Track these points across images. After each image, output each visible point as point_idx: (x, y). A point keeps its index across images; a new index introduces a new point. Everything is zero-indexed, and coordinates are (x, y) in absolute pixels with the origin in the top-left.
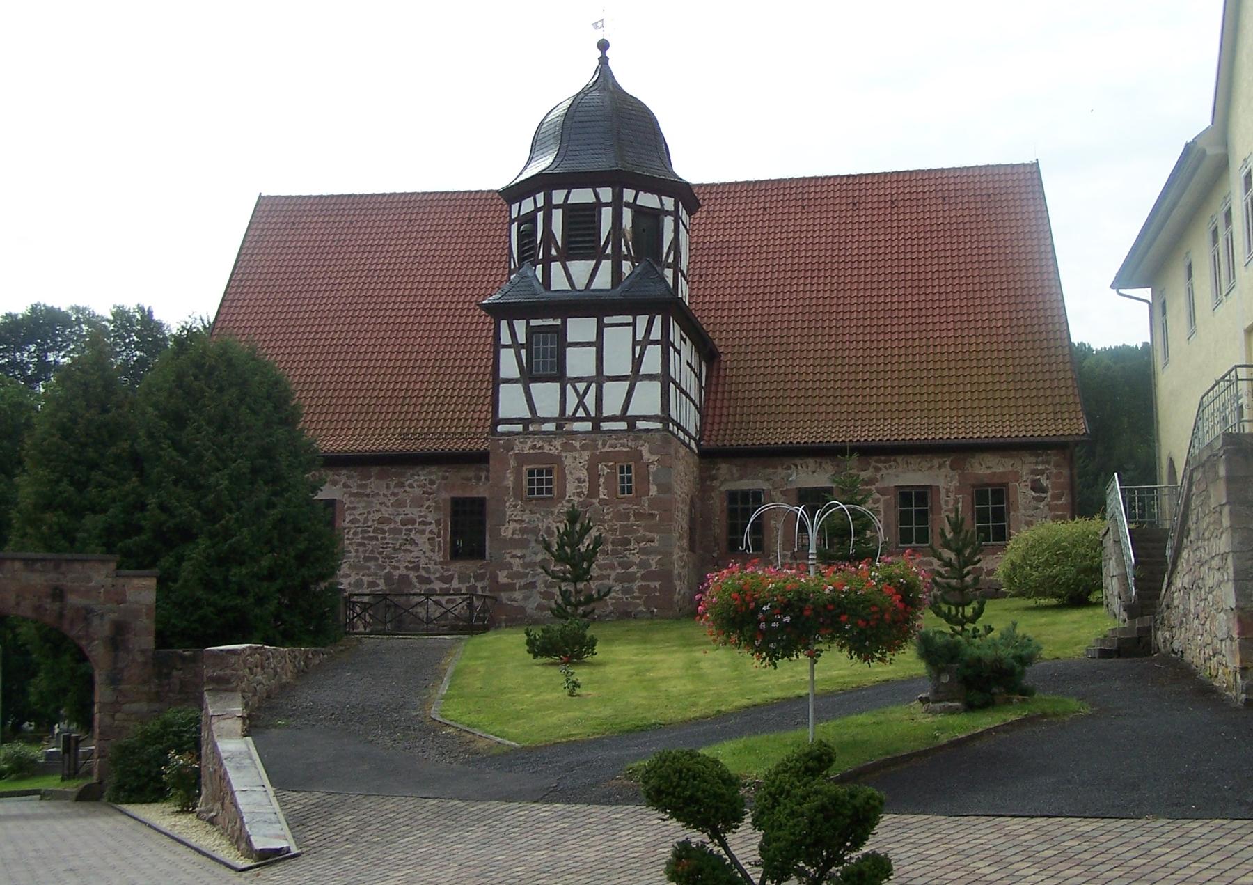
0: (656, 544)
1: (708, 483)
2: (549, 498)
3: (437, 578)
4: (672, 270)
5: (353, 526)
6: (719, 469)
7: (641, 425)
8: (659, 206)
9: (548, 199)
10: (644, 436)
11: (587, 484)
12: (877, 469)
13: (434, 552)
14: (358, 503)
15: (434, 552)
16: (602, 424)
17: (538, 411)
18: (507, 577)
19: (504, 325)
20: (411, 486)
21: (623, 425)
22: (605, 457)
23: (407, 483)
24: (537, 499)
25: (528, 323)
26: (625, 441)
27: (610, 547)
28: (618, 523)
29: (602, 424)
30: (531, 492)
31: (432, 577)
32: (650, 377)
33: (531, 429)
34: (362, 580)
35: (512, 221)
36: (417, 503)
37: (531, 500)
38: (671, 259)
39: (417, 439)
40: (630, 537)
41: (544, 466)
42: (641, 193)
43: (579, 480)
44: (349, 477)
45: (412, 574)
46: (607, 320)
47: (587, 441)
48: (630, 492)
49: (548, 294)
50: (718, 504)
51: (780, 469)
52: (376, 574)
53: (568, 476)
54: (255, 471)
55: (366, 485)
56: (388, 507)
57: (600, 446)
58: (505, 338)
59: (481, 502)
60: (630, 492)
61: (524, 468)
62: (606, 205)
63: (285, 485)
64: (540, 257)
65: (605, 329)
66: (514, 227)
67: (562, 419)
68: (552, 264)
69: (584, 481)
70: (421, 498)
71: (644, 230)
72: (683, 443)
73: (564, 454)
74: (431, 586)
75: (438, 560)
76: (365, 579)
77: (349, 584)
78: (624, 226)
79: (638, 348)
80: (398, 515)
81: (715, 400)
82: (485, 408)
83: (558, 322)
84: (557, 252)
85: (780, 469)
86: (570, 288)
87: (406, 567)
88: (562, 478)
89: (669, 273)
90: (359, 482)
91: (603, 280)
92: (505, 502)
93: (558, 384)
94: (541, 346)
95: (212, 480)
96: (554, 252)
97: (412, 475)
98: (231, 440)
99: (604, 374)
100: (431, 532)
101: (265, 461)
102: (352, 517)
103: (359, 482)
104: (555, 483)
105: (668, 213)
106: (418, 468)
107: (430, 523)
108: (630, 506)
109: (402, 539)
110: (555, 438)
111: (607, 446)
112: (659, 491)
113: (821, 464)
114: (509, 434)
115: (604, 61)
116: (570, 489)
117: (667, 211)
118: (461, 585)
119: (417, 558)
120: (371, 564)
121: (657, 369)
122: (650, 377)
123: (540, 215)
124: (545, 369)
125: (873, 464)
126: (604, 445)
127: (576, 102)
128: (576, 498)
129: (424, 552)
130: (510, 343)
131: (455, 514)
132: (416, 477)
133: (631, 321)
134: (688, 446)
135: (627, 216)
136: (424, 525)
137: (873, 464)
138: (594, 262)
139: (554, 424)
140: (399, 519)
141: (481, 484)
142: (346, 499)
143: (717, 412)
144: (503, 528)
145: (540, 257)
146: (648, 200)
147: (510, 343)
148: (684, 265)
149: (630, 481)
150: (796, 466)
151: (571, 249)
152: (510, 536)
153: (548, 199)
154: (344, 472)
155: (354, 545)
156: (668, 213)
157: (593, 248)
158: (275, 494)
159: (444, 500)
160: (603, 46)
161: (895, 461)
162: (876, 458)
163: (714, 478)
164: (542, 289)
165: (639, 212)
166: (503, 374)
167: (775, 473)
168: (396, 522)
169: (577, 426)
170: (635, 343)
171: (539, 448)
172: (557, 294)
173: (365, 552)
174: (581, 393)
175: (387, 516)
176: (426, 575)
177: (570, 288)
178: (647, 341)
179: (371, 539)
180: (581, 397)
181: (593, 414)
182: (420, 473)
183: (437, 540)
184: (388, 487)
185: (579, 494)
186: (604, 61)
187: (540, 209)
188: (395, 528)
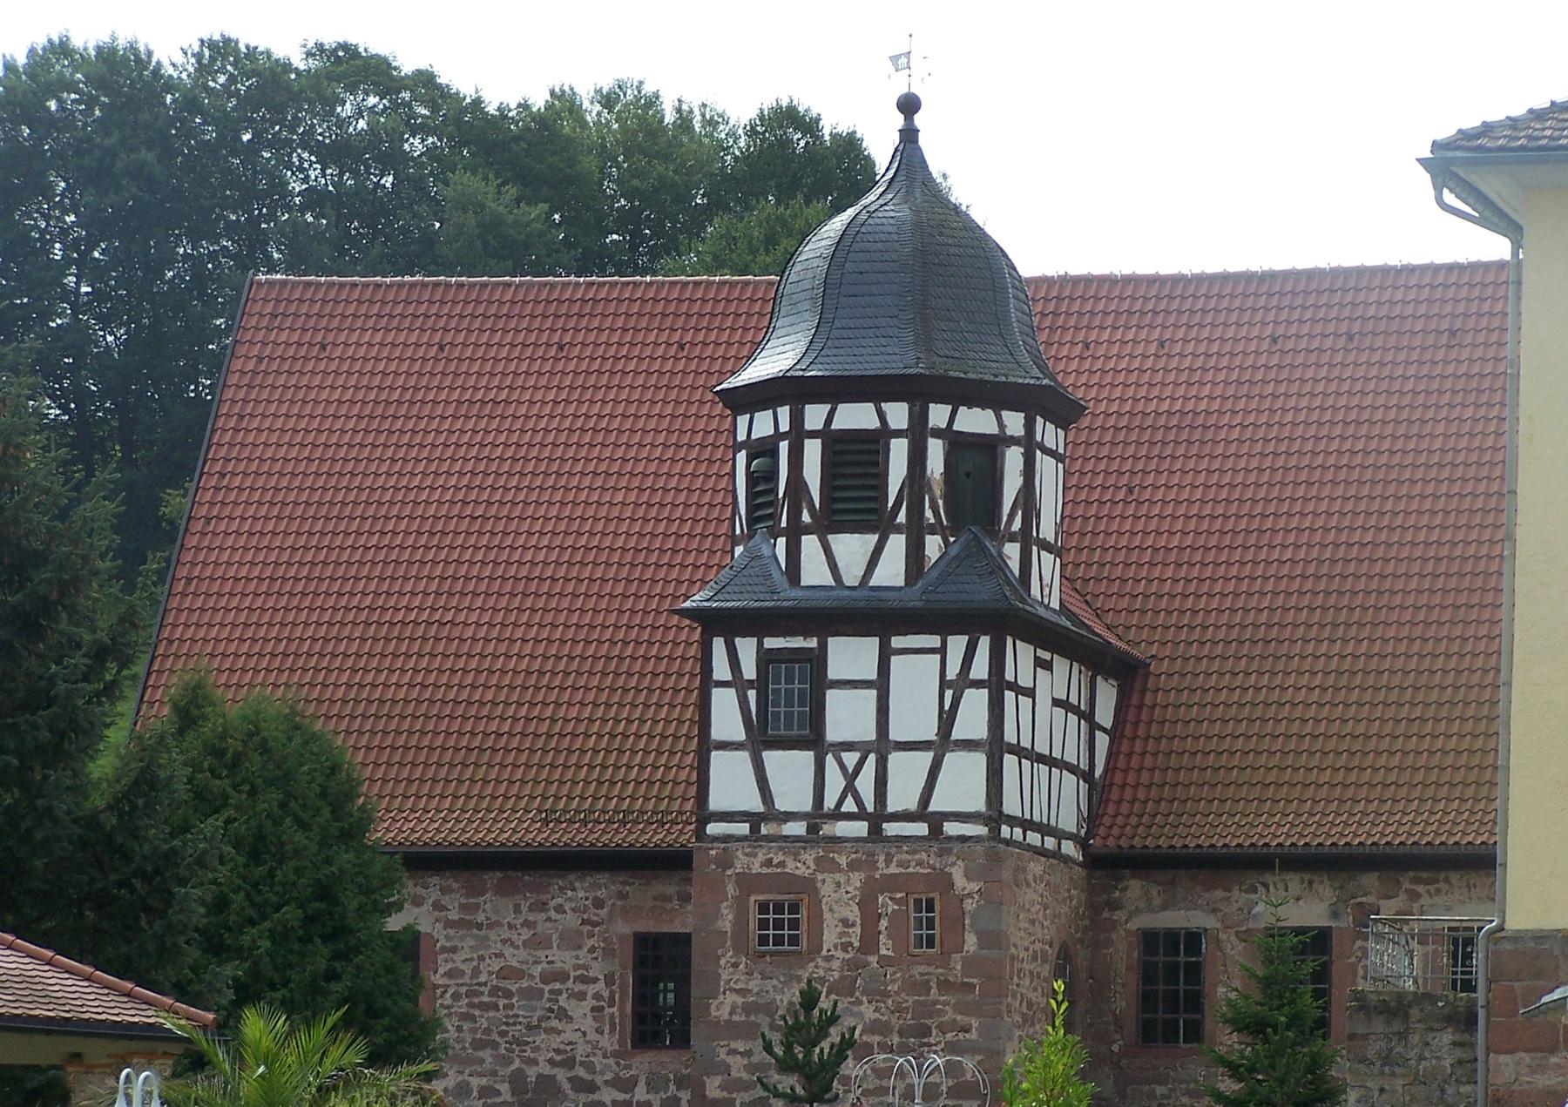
0: (973, 1035)
1: (1106, 914)
2: (794, 952)
3: (606, 1082)
4: (1018, 545)
5: (451, 982)
6: (1125, 889)
7: (951, 828)
8: (995, 430)
9: (797, 419)
10: (957, 847)
11: (858, 929)
12: (1414, 896)
13: (602, 1033)
14: (462, 939)
15: (602, 1033)
16: (885, 825)
17: (776, 800)
18: (722, 1087)
19: (719, 645)
20: (560, 909)
21: (921, 829)
22: (890, 884)
23: (553, 903)
24: (772, 954)
25: (760, 644)
26: (924, 856)
27: (896, 1039)
28: (911, 999)
29: (885, 825)
30: (763, 940)
31: (599, 1080)
32: (969, 745)
33: (764, 831)
34: (468, 1083)
35: (738, 447)
36: (572, 941)
37: (762, 955)
38: (1016, 526)
39: (571, 822)
40: (929, 1022)
41: (786, 897)
42: (963, 409)
43: (846, 923)
44: (445, 890)
45: (561, 1075)
46: (897, 642)
47: (859, 855)
48: (931, 944)
49: (794, 593)
50: (1123, 955)
51: (1236, 893)
52: (494, 1073)
53: (827, 915)
54: (309, 920)
55: (477, 906)
56: (517, 948)
57: (881, 864)
58: (721, 670)
59: (685, 940)
60: (931, 944)
61: (752, 899)
62: (898, 434)
63: (353, 942)
64: (784, 524)
65: (893, 658)
66: (742, 457)
67: (817, 816)
68: (803, 537)
69: (853, 925)
70: (579, 933)
71: (968, 475)
72: (1041, 852)
73: (820, 877)
74: (595, 1097)
75: (610, 1049)
76: (475, 1082)
77: (445, 1090)
78: (929, 472)
79: (949, 694)
80: (536, 962)
81: (1130, 755)
82: (683, 775)
83: (813, 643)
84: (811, 517)
85: (1236, 893)
86: (833, 584)
87: (551, 1062)
88: (817, 918)
89: (1012, 551)
90: (463, 901)
91: (891, 570)
92: (719, 958)
93: (812, 753)
94: (783, 686)
95: (246, 940)
96: (806, 517)
97: (561, 889)
98: (271, 874)
99: (891, 737)
100: (597, 996)
101: (323, 906)
102: (450, 965)
103: (463, 901)
104: (804, 926)
105: (1014, 441)
106: (572, 877)
107: (596, 980)
108: (931, 969)
109: (543, 1008)
110: (805, 848)
111: (894, 864)
112: (981, 944)
113: (1311, 883)
114: (727, 838)
115: (909, 135)
116: (830, 937)
117: (1012, 437)
118: (650, 1097)
119: (570, 1043)
120: (486, 1054)
121: (980, 731)
122: (969, 745)
123: (784, 446)
124: (789, 726)
125: (1407, 885)
126: (888, 861)
127: (851, 232)
128: (840, 954)
129: (584, 1034)
130: (729, 678)
131: (640, 962)
132: (570, 893)
133: (939, 645)
134: (1056, 855)
135: (936, 452)
136: (582, 982)
137: (1407, 885)
138: (877, 536)
139: (804, 824)
140: (537, 970)
141: (689, 908)
142: (438, 932)
143: (1131, 780)
144: (715, 1003)
145: (784, 524)
146: (976, 421)
147: (729, 678)
148: (1047, 530)
149: (931, 926)
150: (1266, 886)
151: (835, 512)
152: (726, 1017)
153: (797, 419)
154: (435, 880)
155: (455, 1019)
156: (1014, 441)
157: (875, 511)
158: (337, 956)
159: (622, 937)
160: (909, 105)
161: (1447, 880)
162: (1411, 874)
163: (1115, 906)
164: (787, 586)
165: (957, 443)
166: (717, 733)
167: (1227, 899)
168: (532, 977)
169: (843, 828)
170: (944, 684)
171: (777, 866)
172: (809, 593)
173: (473, 1031)
174: (850, 771)
175: (515, 964)
176: (588, 1077)
177: (833, 584)
178: (965, 681)
179: (484, 1007)
180: (851, 778)
181: (870, 808)
182: (577, 885)
183: (608, 1010)
184: (517, 909)
185: (845, 947)
186: (909, 135)
187: (783, 436)
188: (530, 988)
